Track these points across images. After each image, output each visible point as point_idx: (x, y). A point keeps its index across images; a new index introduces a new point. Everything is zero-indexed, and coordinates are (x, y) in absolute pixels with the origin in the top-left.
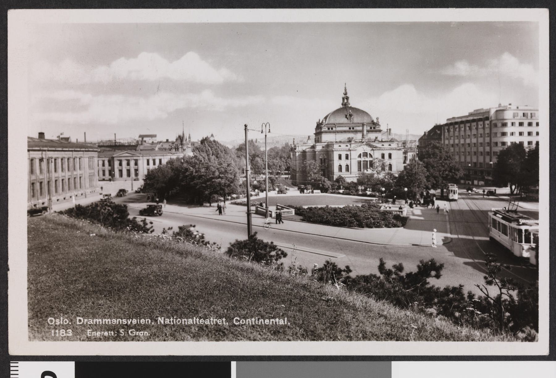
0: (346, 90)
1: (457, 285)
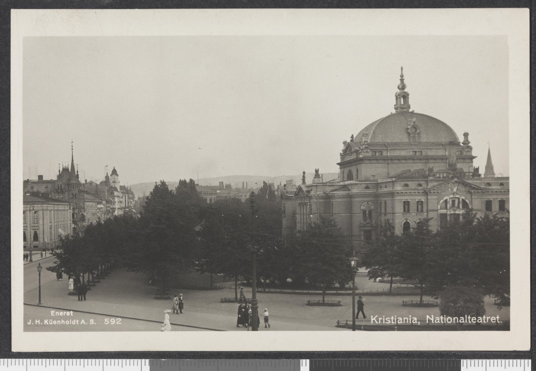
0: (402, 80)
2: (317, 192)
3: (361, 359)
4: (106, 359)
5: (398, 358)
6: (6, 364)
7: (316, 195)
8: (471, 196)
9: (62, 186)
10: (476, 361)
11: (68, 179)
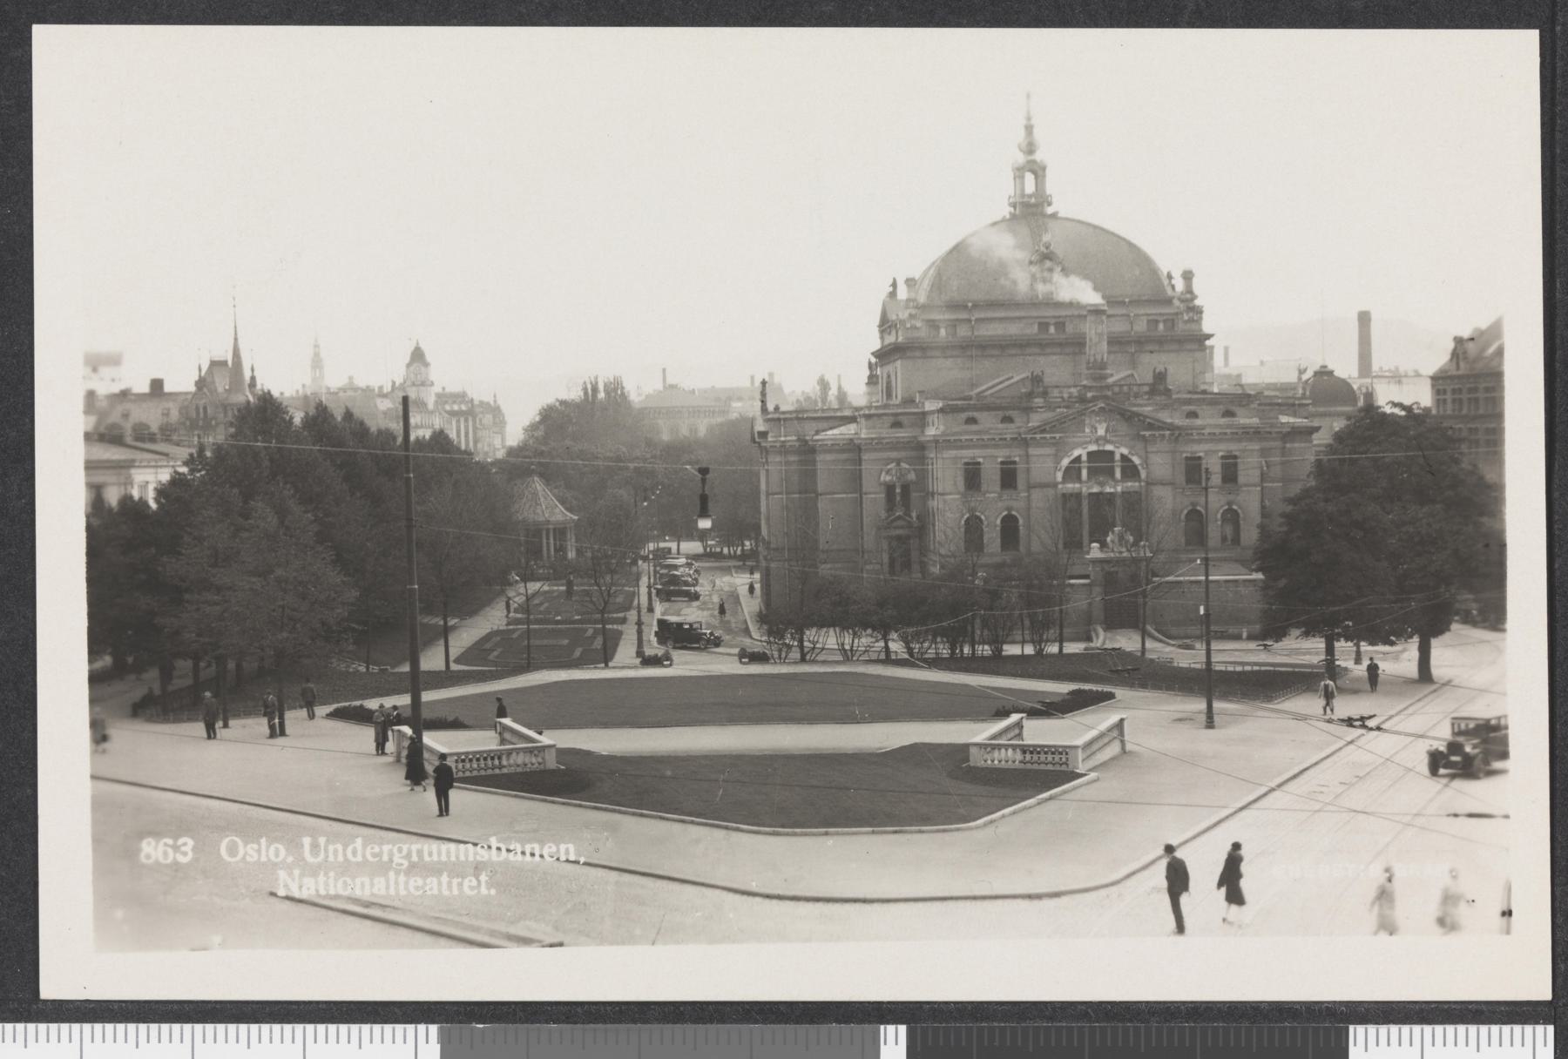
0: (1029, 129)
2: (780, 436)
3: (1059, 1024)
4: (314, 1023)
5: (1166, 1021)
6: (20, 1038)
7: (778, 445)
8: (1146, 448)
9: (208, 408)
10: (1394, 1028)
11: (225, 389)
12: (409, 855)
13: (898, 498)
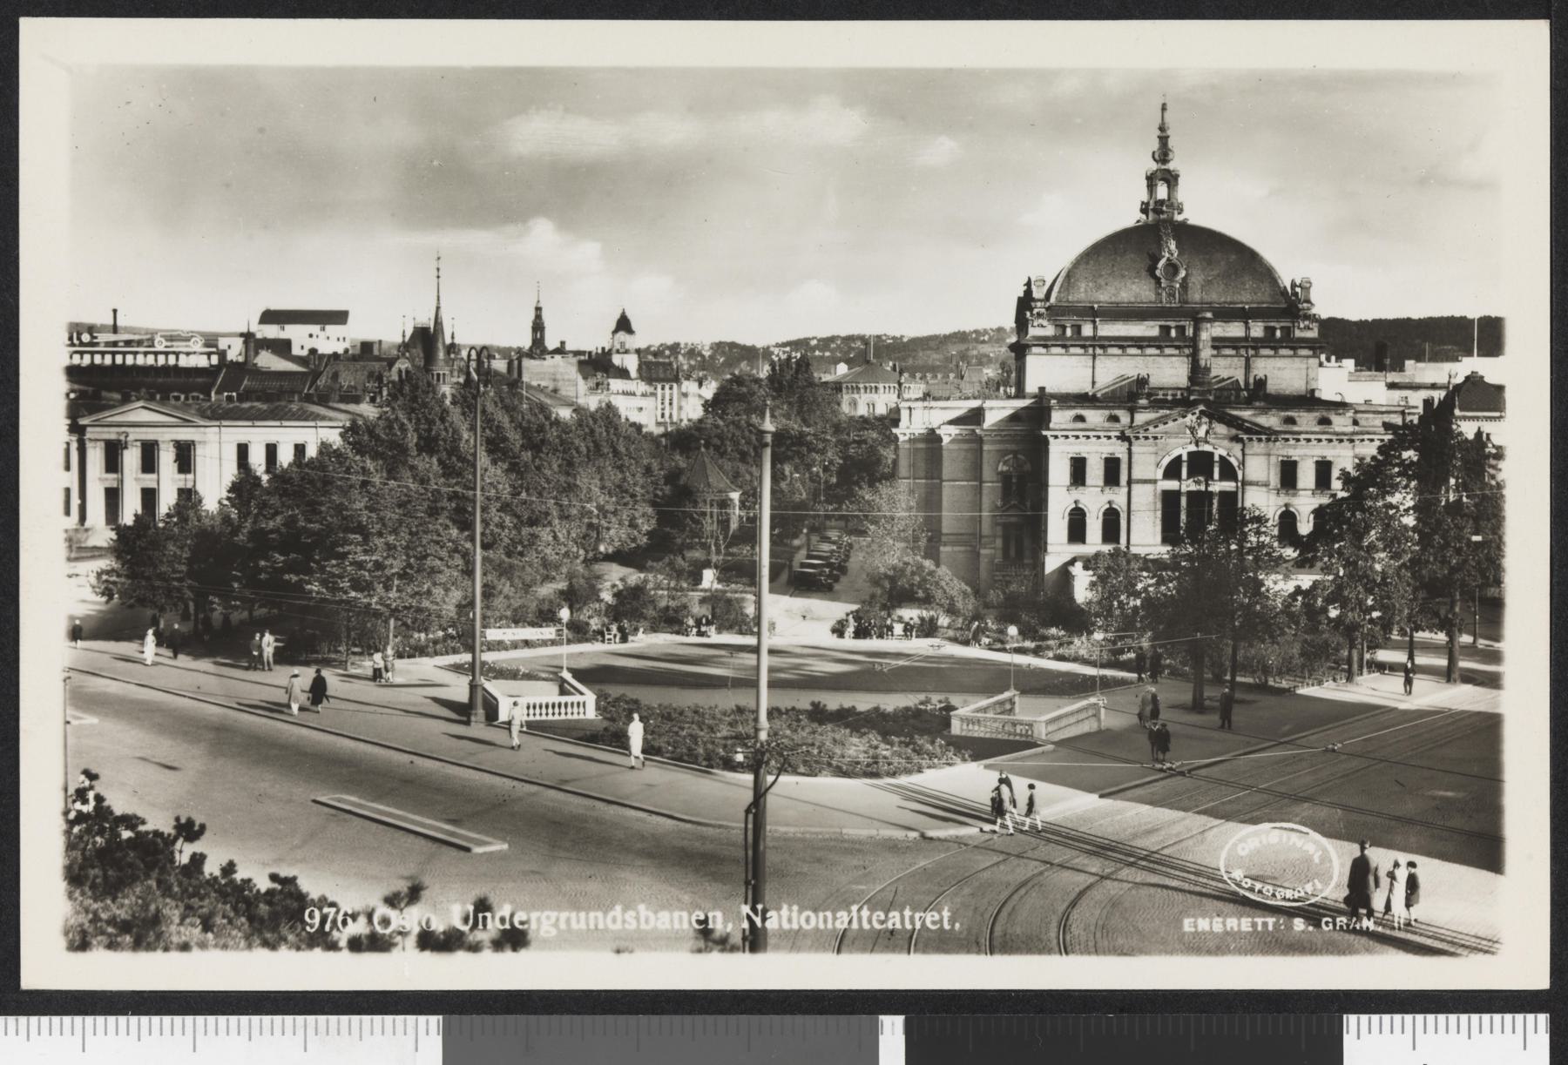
0: (1164, 140)
1: (291, 875)
12: (556, 925)
13: (1014, 488)
